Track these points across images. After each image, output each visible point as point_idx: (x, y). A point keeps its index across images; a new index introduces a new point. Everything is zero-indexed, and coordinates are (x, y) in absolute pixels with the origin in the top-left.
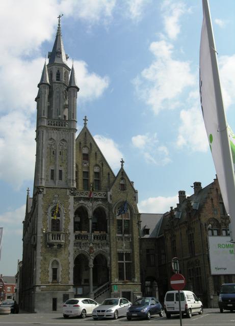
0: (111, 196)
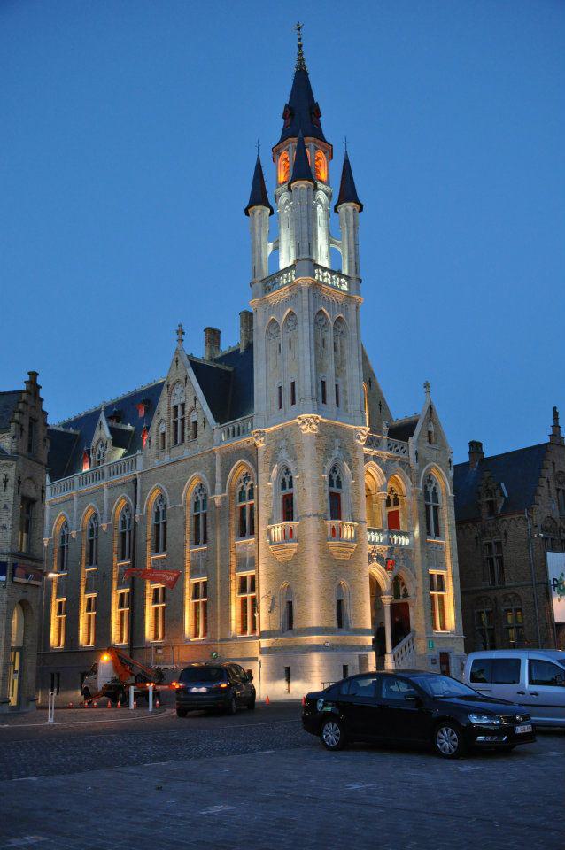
0: (417, 454)
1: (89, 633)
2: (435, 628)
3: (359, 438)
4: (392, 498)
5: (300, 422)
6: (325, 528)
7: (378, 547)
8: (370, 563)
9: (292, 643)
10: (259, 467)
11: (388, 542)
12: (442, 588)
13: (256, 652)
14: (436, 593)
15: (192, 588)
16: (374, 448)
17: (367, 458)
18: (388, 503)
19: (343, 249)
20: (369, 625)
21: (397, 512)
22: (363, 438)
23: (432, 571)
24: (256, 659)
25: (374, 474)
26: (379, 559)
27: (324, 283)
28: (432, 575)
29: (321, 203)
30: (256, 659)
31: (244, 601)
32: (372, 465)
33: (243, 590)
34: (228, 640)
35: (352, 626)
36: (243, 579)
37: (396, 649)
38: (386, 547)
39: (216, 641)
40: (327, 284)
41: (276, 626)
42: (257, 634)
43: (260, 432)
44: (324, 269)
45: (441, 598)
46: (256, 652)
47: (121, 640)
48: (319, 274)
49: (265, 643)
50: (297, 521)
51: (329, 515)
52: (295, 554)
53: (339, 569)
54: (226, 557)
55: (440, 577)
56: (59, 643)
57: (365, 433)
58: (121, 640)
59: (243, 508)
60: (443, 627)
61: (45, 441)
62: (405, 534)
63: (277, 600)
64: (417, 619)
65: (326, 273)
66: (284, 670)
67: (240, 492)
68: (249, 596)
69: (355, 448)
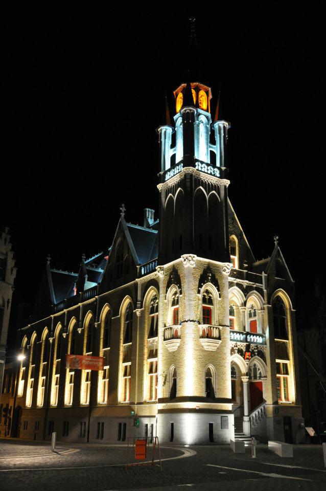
1: (125, 393)
2: (280, 398)
3: (225, 271)
4: (252, 311)
5: (183, 260)
6: (198, 330)
7: (239, 343)
8: (231, 354)
9: (175, 407)
10: (160, 290)
11: (246, 340)
12: (287, 373)
13: (155, 413)
14: (282, 376)
15: (123, 369)
16: (256, 282)
17: (231, 284)
18: (250, 316)
19: (217, 151)
20: (229, 396)
21: (255, 321)
22: (227, 271)
23: (278, 361)
24: (154, 417)
25: (239, 298)
26: (240, 352)
27: (202, 172)
28: (279, 364)
29: (202, 122)
30: (154, 417)
31: (151, 378)
32: (254, 293)
33: (151, 371)
34: (141, 403)
35: (217, 396)
36: (152, 364)
37: (255, 413)
38: (245, 344)
39: (135, 404)
40: (204, 172)
41: (167, 395)
42: (157, 400)
43: (160, 268)
44: (202, 163)
45: (286, 380)
46: (155, 413)
47: (125, 399)
48: (198, 165)
49: (161, 406)
50: (180, 324)
51: (201, 321)
52: (179, 347)
53: (210, 359)
54: (142, 349)
55: (285, 365)
56: (104, 400)
57: (229, 267)
58: (125, 399)
59: (153, 318)
60: (287, 398)
61: (12, 270)
62: (260, 335)
63: (168, 378)
64: (268, 395)
65: (204, 165)
66: (118, 425)
67: (152, 308)
68: (154, 375)
69: (222, 277)
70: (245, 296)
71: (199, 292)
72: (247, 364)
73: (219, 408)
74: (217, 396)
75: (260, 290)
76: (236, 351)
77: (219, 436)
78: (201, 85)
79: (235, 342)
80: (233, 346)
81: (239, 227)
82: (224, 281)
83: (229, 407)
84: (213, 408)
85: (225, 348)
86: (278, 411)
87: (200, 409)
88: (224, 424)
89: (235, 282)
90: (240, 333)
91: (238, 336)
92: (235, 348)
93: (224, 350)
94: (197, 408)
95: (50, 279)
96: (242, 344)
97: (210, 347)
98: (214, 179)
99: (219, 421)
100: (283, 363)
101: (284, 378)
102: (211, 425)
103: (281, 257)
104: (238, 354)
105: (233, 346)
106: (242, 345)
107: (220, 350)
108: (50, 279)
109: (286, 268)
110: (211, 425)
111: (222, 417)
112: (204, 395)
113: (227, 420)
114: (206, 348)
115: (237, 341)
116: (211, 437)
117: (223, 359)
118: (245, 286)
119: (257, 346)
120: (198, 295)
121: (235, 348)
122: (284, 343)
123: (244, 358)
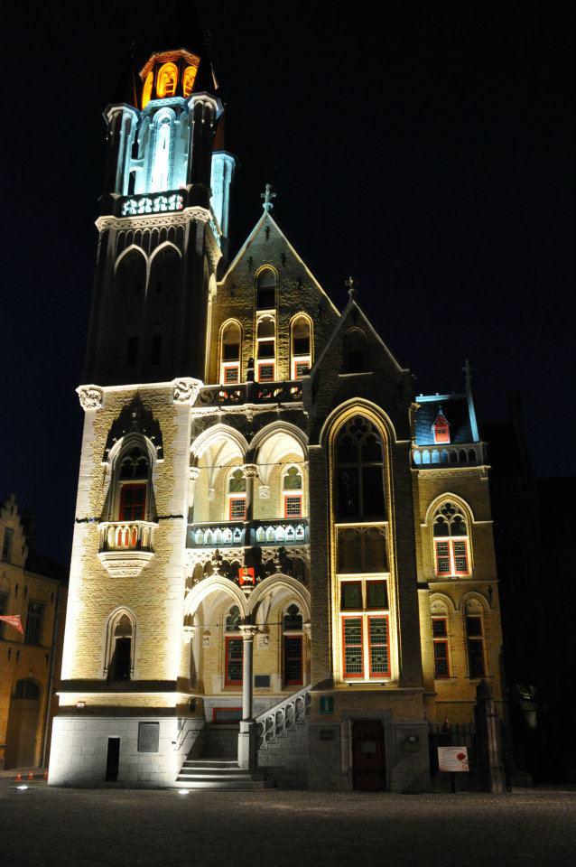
26: (230, 571)
70: (249, 439)
71: (105, 458)
72: (247, 595)
73: (140, 704)
74: (136, 675)
75: (290, 416)
76: (216, 569)
77: (130, 767)
78: (162, 54)
79: (214, 550)
80: (210, 559)
81: (318, 290)
82: (175, 420)
83: (173, 699)
84: (124, 704)
85: (165, 566)
86: (331, 708)
87: (86, 706)
88: (148, 741)
89: (220, 414)
90: (232, 526)
91: (226, 535)
92: (213, 563)
93: (164, 571)
94: (79, 705)
95: (470, 569)
96: (235, 550)
97: (120, 570)
98: (166, 219)
99: (135, 734)
100: (367, 582)
101: (372, 622)
102: (114, 745)
103: (365, 323)
104: (222, 575)
105: (210, 559)
106: (236, 555)
107: (152, 575)
108: (470, 569)
109: (381, 345)
110: (114, 745)
111: (140, 723)
112: (101, 675)
113: (157, 731)
114: (112, 573)
115: (218, 545)
116: (111, 768)
117: (160, 591)
118: (249, 418)
119: (280, 550)
120: (104, 464)
121: (213, 563)
122: (374, 529)
123: (238, 583)
